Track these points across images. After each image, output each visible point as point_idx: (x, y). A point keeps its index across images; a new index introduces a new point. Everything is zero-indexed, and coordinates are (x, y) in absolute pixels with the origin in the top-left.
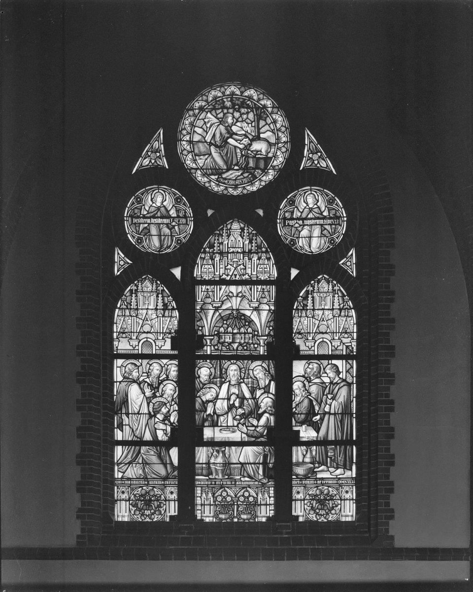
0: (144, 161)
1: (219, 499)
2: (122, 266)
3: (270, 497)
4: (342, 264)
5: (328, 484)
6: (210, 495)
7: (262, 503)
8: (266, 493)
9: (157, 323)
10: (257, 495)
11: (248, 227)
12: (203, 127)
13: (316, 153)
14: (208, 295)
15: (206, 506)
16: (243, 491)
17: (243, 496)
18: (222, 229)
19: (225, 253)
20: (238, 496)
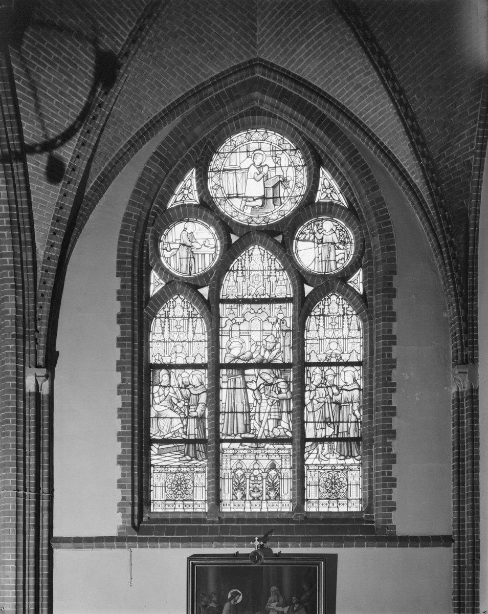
12: (172, 248)
14: (281, 312)
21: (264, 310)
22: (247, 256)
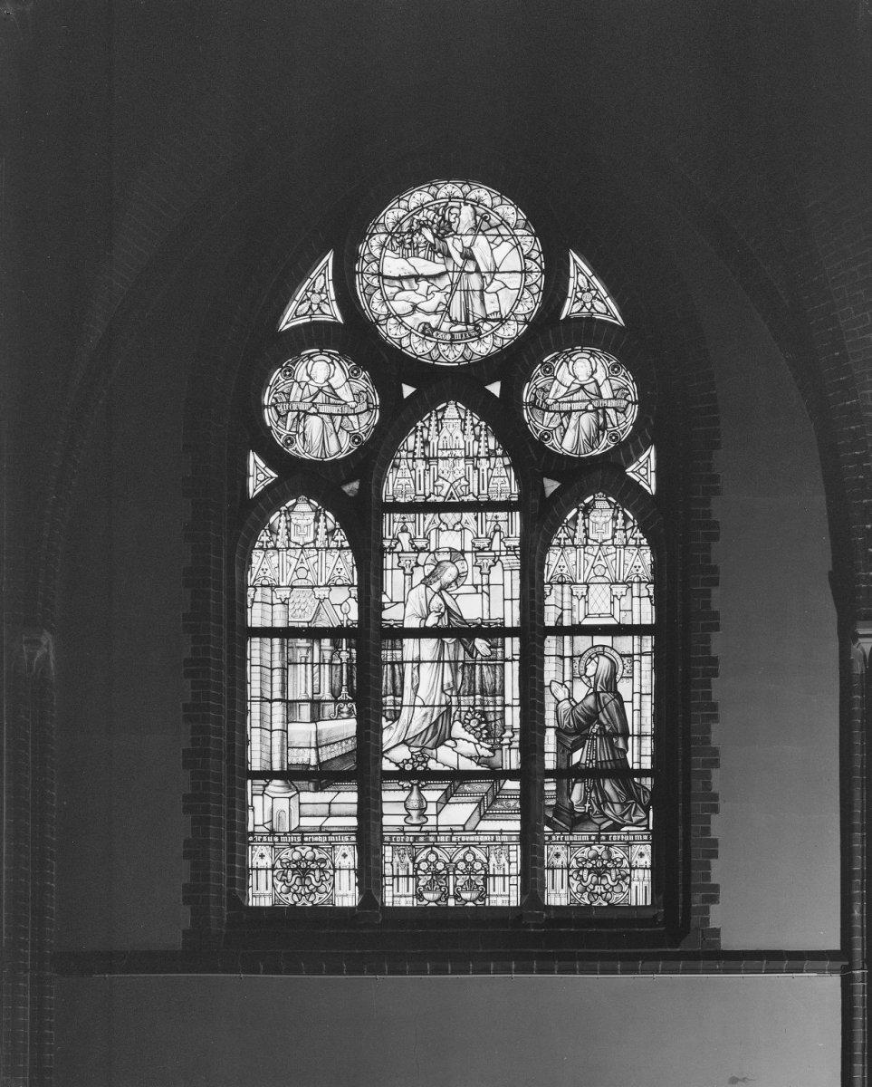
0: (300, 307)
1: (424, 866)
2: (261, 482)
3: (510, 863)
4: (632, 472)
5: (311, 842)
6: (407, 859)
7: (400, 874)
8: (503, 856)
9: (614, 562)
10: (488, 859)
11: (471, 415)
13: (589, 291)
15: (497, 878)
16: (463, 852)
17: (464, 860)
18: (429, 419)
19: (433, 458)
20: (454, 861)
21: (466, 526)
22: (433, 423)
